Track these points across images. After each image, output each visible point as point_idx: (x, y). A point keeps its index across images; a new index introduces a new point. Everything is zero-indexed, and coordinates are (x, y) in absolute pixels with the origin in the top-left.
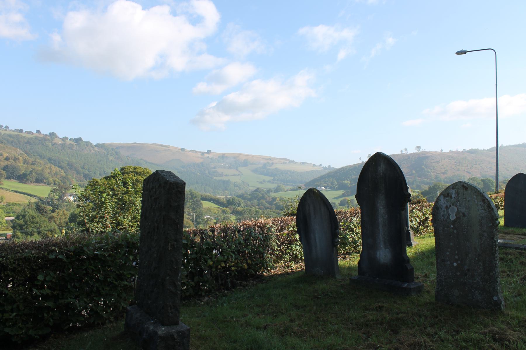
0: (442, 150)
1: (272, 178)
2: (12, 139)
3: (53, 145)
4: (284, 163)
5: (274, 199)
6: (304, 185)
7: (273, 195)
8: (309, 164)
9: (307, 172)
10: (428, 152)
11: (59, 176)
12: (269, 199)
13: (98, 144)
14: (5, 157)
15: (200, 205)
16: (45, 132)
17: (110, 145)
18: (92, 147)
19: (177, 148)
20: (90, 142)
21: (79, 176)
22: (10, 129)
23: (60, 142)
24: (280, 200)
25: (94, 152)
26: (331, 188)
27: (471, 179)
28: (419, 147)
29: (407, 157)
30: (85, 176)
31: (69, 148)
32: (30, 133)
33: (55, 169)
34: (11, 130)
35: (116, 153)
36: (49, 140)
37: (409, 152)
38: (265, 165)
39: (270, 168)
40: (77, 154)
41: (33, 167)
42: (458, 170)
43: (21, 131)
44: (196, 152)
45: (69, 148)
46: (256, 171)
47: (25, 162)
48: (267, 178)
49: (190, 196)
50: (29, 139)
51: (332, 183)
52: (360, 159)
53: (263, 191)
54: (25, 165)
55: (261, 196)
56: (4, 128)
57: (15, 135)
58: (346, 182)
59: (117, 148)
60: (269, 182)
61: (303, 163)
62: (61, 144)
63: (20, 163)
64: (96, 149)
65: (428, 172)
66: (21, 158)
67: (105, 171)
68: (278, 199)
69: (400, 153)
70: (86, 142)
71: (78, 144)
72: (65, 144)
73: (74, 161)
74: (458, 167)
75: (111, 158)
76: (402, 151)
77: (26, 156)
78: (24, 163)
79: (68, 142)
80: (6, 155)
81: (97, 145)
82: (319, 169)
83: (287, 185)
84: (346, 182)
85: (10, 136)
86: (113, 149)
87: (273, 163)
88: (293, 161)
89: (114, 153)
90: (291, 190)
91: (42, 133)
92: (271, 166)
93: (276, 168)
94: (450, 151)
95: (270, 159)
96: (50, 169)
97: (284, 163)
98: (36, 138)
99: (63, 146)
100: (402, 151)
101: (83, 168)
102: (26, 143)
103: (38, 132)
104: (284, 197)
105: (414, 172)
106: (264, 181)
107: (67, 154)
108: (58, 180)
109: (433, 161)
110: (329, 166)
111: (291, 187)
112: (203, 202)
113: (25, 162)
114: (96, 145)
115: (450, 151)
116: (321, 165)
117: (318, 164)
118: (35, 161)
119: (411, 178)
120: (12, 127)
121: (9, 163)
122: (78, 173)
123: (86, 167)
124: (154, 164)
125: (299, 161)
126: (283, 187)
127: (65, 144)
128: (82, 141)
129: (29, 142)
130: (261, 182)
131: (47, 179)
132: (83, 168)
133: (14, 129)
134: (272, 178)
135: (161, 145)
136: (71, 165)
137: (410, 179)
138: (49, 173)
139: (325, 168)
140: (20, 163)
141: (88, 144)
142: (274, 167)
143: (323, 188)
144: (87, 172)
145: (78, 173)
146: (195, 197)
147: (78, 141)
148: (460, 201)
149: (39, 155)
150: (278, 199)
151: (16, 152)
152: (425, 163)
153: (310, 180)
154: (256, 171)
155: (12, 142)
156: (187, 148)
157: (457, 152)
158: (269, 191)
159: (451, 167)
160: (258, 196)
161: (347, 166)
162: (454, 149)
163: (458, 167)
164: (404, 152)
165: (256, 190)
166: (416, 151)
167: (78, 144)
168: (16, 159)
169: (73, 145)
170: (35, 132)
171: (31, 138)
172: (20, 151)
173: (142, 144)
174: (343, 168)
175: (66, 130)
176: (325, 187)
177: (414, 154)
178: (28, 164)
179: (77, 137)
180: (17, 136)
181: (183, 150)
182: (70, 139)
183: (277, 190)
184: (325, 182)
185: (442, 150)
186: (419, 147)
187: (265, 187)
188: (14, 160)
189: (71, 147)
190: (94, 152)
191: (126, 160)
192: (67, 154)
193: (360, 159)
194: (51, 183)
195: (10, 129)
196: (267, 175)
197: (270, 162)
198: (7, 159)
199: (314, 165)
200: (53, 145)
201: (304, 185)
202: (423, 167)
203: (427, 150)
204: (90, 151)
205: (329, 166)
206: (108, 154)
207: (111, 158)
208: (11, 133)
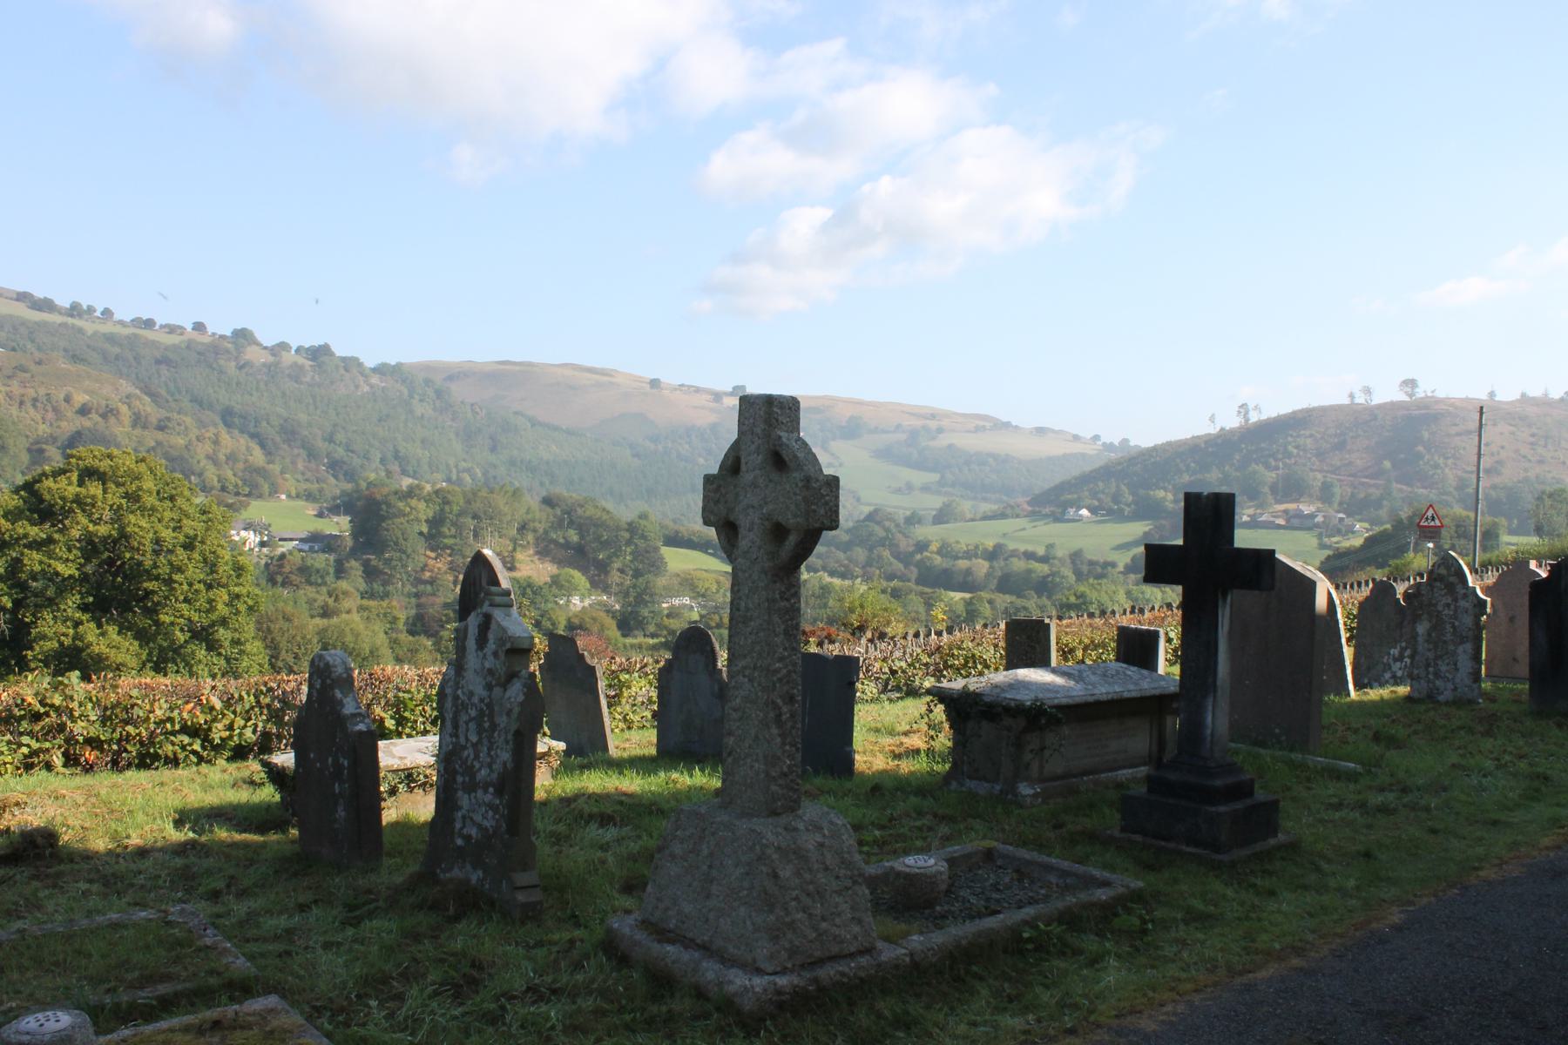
0: (1492, 394)
1: (935, 477)
2: (117, 350)
3: (241, 368)
4: (977, 429)
5: (922, 546)
6: (1029, 503)
7: (929, 532)
8: (1060, 432)
9: (1050, 459)
10: (1439, 401)
11: (241, 465)
12: (905, 545)
13: (384, 365)
14: (77, 406)
15: (657, 565)
16: (221, 325)
17: (428, 367)
18: (362, 374)
19: (639, 379)
20: (356, 359)
21: (313, 465)
22: (117, 317)
23: (261, 358)
24: (939, 552)
25: (366, 389)
26: (1110, 512)
27: (1551, 496)
28: (1410, 383)
29: (826, 405)
30: (335, 466)
31: (289, 376)
32: (172, 329)
33: (231, 441)
34: (121, 323)
35: (439, 394)
36: (228, 351)
37: (1378, 399)
38: (914, 434)
39: (932, 444)
40: (314, 397)
41: (160, 436)
42: (1541, 462)
43: (149, 324)
44: (698, 390)
45: (289, 376)
46: (885, 454)
47: (138, 420)
48: (919, 478)
49: (627, 535)
50: (166, 349)
51: (1116, 498)
52: (1212, 419)
53: (891, 520)
54: (138, 431)
55: (882, 533)
56: (98, 314)
57: (128, 337)
58: (1161, 494)
59: (450, 378)
60: (925, 489)
61: (1041, 431)
62: (264, 365)
63: (120, 423)
64: (375, 380)
65: (1436, 466)
66: (124, 409)
67: (397, 452)
68: (934, 547)
69: (1347, 401)
70: (344, 359)
71: (320, 366)
72: (276, 364)
73: (303, 417)
74: (1540, 450)
75: (419, 409)
76: (1352, 396)
77: (147, 406)
78: (134, 426)
79: (289, 358)
80: (80, 398)
81: (381, 370)
82: (1090, 450)
83: (985, 500)
84: (1161, 494)
85: (111, 338)
86: (428, 382)
87: (940, 430)
88: (1007, 425)
89: (430, 392)
90: (985, 518)
91: (210, 330)
92: (934, 438)
93: (950, 446)
94: (1523, 395)
95: (933, 416)
96: (216, 442)
97: (977, 429)
98: (190, 345)
99: (272, 370)
100: (1352, 396)
101: (331, 440)
102: (158, 362)
103: (199, 327)
104: (952, 540)
105: (1387, 464)
106: (910, 487)
107: (284, 394)
108: (233, 479)
109: (1453, 430)
110: (1125, 441)
111: (986, 507)
112: (668, 553)
113: (138, 420)
114: (375, 370)
115: (1523, 395)
116: (1096, 438)
117: (1087, 434)
118: (168, 419)
119: (1376, 486)
120: (124, 313)
121: (88, 424)
122: (312, 455)
123: (340, 437)
124: (556, 429)
125: (1027, 421)
126: (966, 506)
127: (276, 364)
128: (332, 354)
129: (165, 359)
130: (898, 491)
131: (200, 475)
132: (331, 440)
133: (128, 319)
134: (935, 477)
135: (591, 370)
136: (290, 433)
137: (1371, 490)
138: (208, 457)
139: (1109, 447)
140: (120, 423)
141: (350, 364)
142: (943, 441)
143: (1084, 512)
144: (340, 452)
145: (312, 455)
146: (644, 537)
147: (319, 354)
148: (10, 671)
149: (194, 400)
150: (934, 547)
151: (115, 390)
152: (1426, 435)
153: (1047, 486)
154: (885, 454)
155: (117, 358)
156: (670, 378)
157: (1544, 403)
158: (913, 520)
159: (1517, 451)
160: (871, 534)
161: (1169, 444)
162: (1535, 392)
163: (1540, 450)
164: (1360, 399)
165: (870, 517)
166: (1400, 396)
167: (320, 366)
168: (108, 413)
169: (301, 368)
170: (189, 328)
171: (175, 347)
172: (126, 387)
173: (530, 364)
174: (1155, 448)
175: (284, 320)
176: (1092, 510)
177: (1392, 406)
178: (145, 427)
179: (317, 342)
180: (132, 341)
181: (655, 383)
182: (298, 350)
183: (941, 517)
184: (1094, 495)
185: (1492, 394)
186: (1410, 383)
187: (899, 506)
188: (104, 416)
189: (296, 373)
190: (366, 389)
191: (469, 415)
192: (284, 394)
193: (1212, 419)
194: (212, 488)
195: (117, 317)
196: (920, 466)
197: (933, 424)
198: (84, 411)
199: (1076, 438)
200: (241, 368)
201: (1029, 503)
202: (1420, 448)
203: (1441, 394)
204: (357, 387)
205: (1125, 441)
206: (411, 396)
207: (419, 409)
208: (118, 329)
